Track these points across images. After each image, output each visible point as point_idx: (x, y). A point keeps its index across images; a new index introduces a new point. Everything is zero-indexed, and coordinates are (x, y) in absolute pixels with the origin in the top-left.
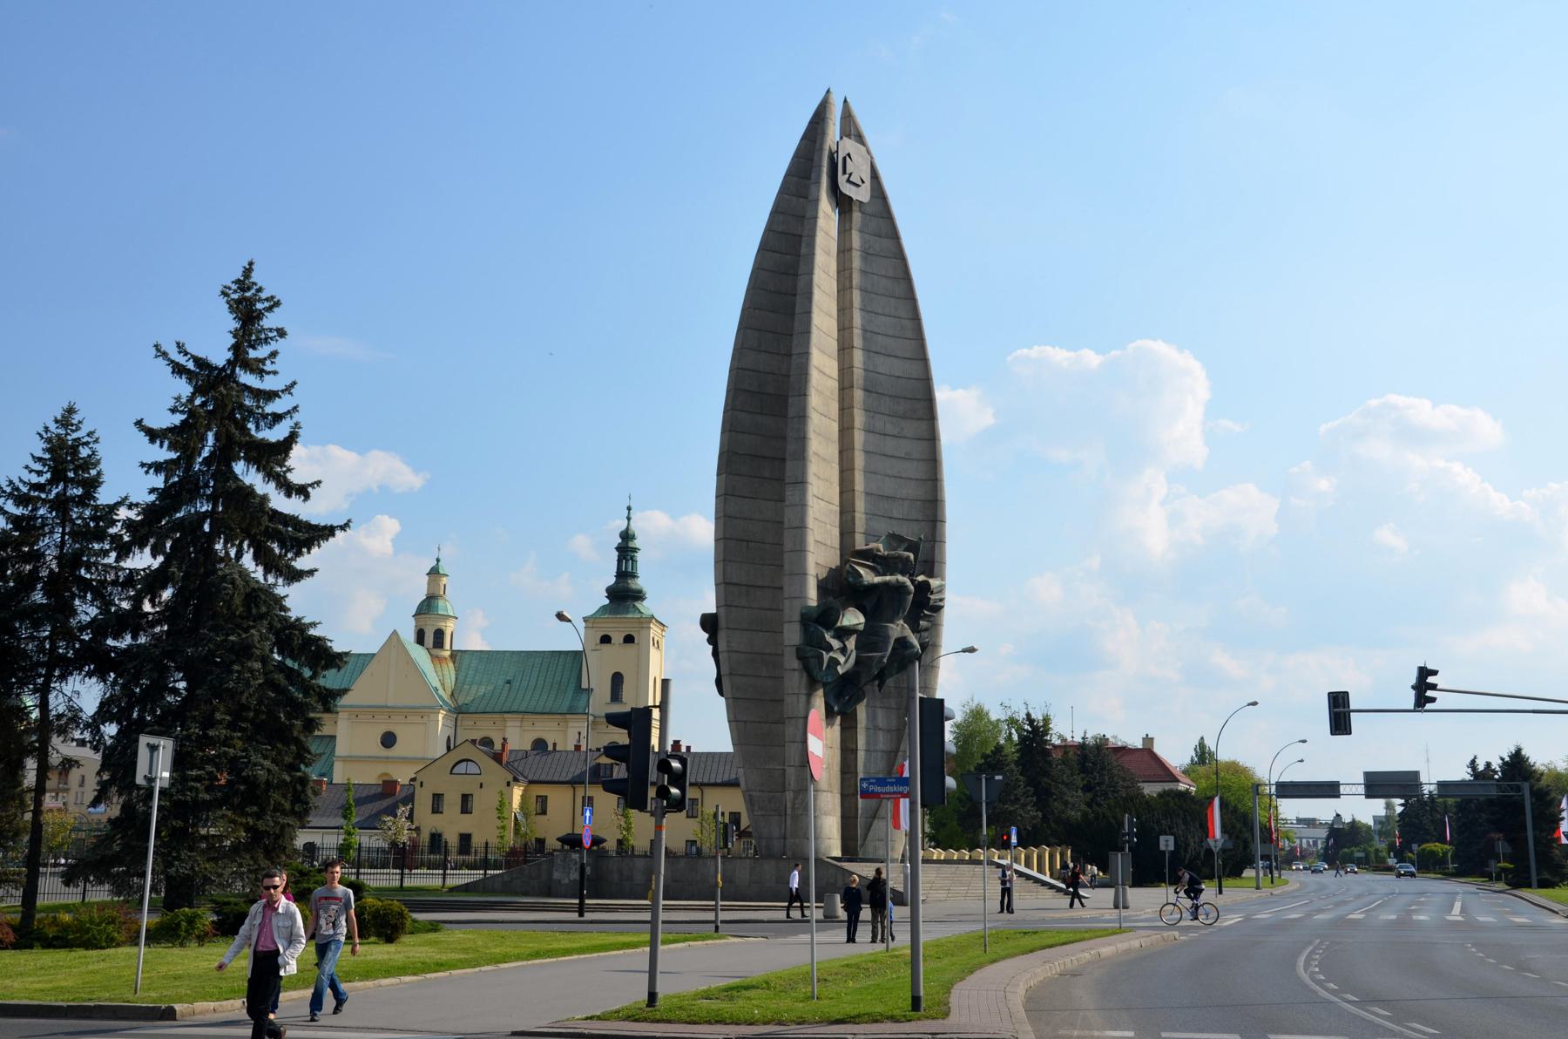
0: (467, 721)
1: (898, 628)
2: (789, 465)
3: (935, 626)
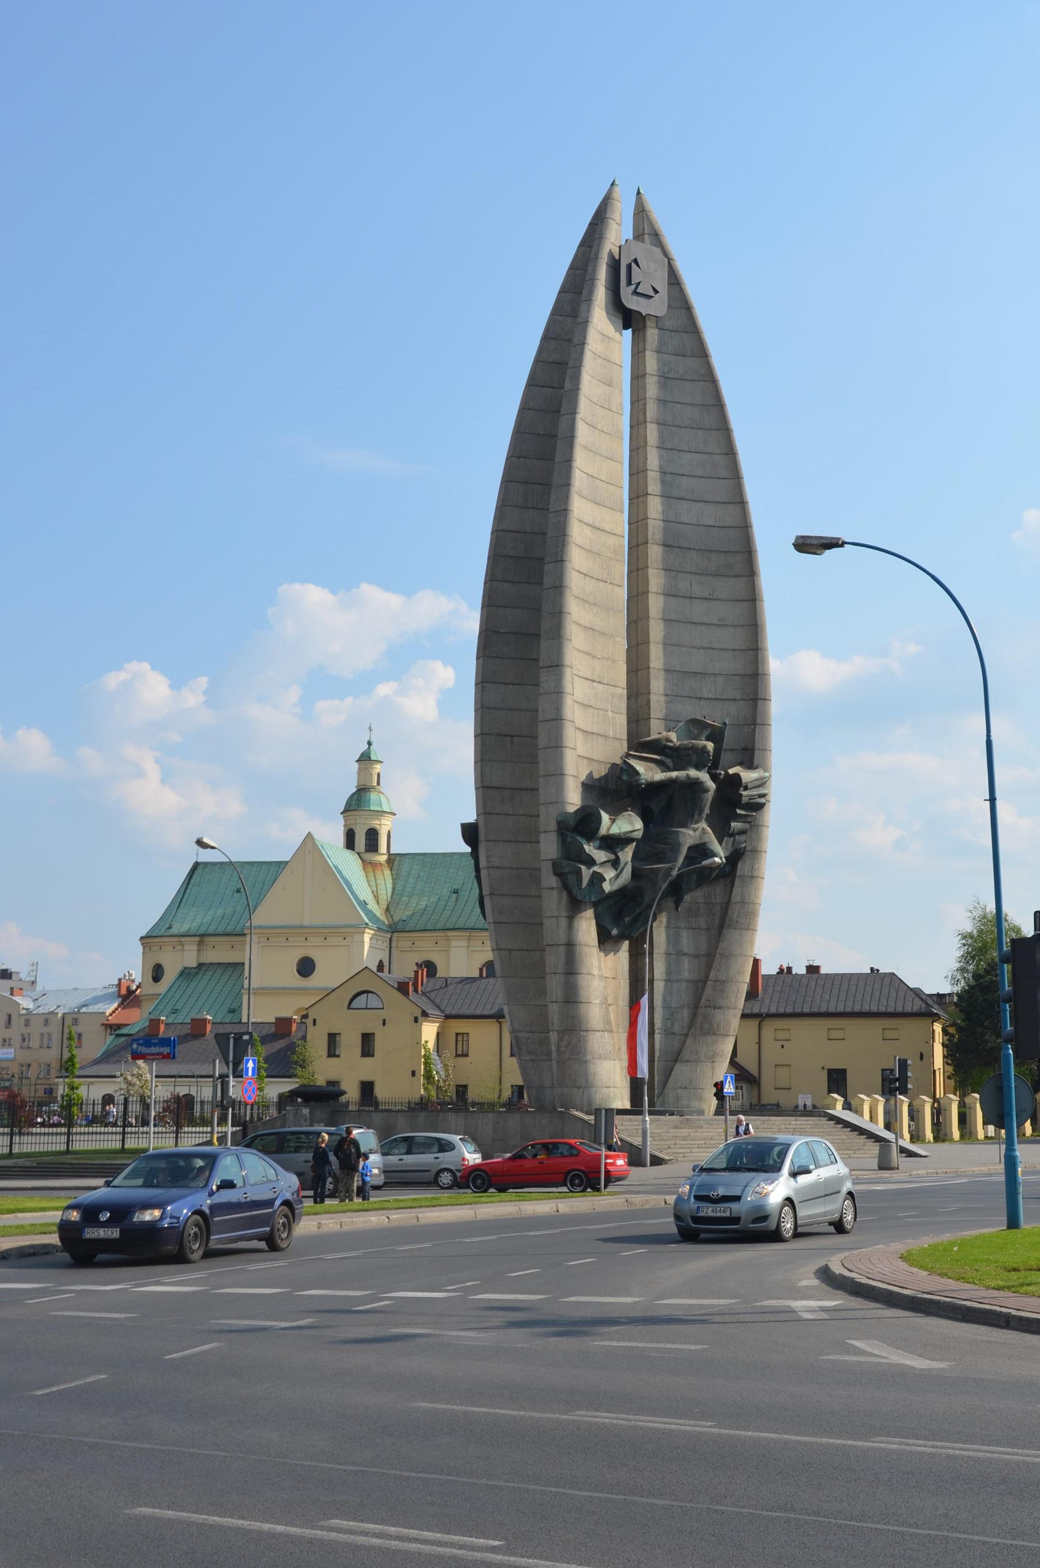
0: (403, 941)
1: (697, 832)
2: (543, 644)
3: (754, 828)
